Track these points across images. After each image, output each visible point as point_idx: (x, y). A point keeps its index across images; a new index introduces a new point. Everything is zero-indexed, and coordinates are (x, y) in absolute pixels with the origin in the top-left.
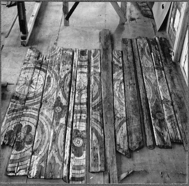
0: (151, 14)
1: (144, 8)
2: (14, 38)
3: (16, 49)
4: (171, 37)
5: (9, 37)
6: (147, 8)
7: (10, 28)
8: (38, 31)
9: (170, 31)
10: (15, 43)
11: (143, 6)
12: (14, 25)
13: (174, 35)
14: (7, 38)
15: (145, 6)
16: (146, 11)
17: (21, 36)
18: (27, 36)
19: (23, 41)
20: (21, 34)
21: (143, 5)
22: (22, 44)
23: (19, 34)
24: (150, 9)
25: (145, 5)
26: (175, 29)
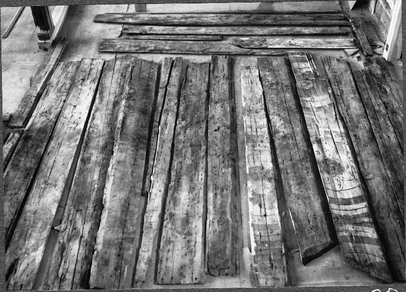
0: (378, 260)
1: (350, 228)
2: (21, 38)
3: (28, 56)
4: (382, 19)
5: (10, 36)
6: (366, 229)
7: (12, 21)
8: (77, 24)
9: (378, 8)
10: (24, 47)
11: (347, 219)
12: (22, 15)
13: (387, 15)
14: (7, 39)
15: (355, 217)
16: (360, 240)
17: (39, 34)
18: (52, 32)
19: (43, 41)
20: (38, 30)
21: (349, 213)
22: (40, 48)
23: (34, 32)
24: (375, 236)
25: (359, 212)
26: (390, 4)
